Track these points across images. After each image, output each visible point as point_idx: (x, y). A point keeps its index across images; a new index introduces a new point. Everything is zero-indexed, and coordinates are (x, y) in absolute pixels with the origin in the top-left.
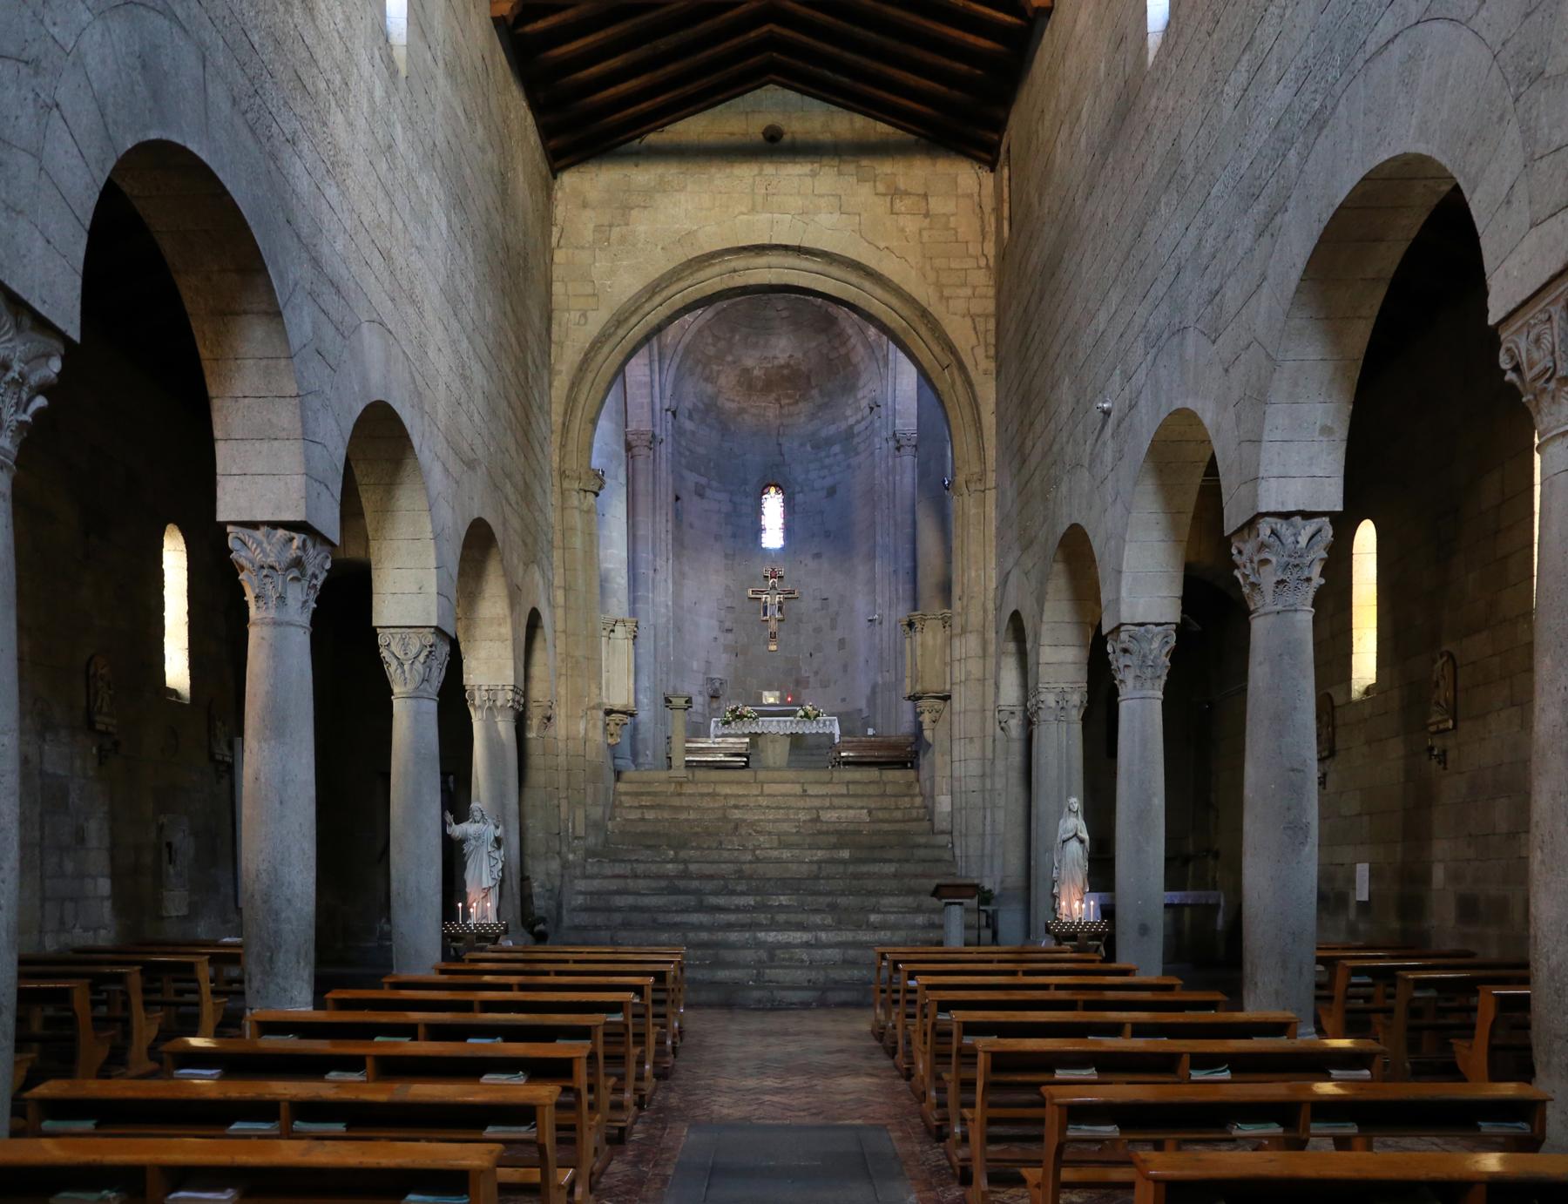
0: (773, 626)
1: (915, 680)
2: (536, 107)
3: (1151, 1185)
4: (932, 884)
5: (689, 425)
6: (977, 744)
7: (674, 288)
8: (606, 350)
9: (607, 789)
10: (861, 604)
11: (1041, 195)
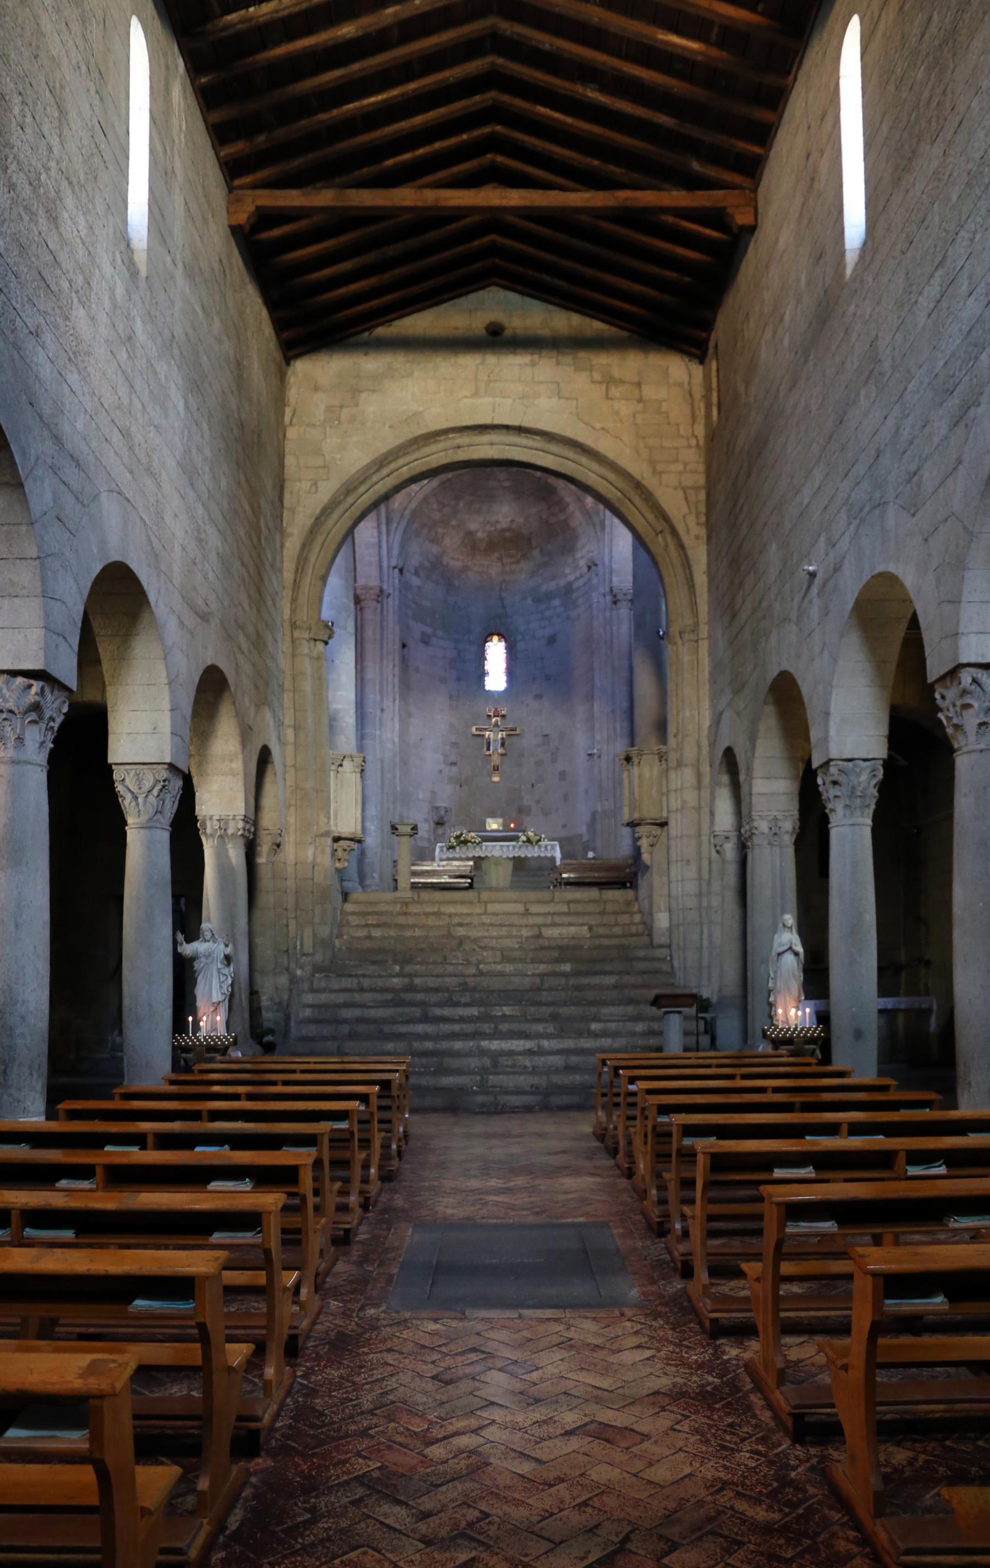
0: (496, 760)
1: (633, 807)
2: (271, 304)
3: (869, 1279)
4: (653, 993)
5: (415, 581)
6: (693, 867)
7: (401, 462)
8: (335, 515)
9: (335, 909)
10: (581, 740)
11: (747, 386)
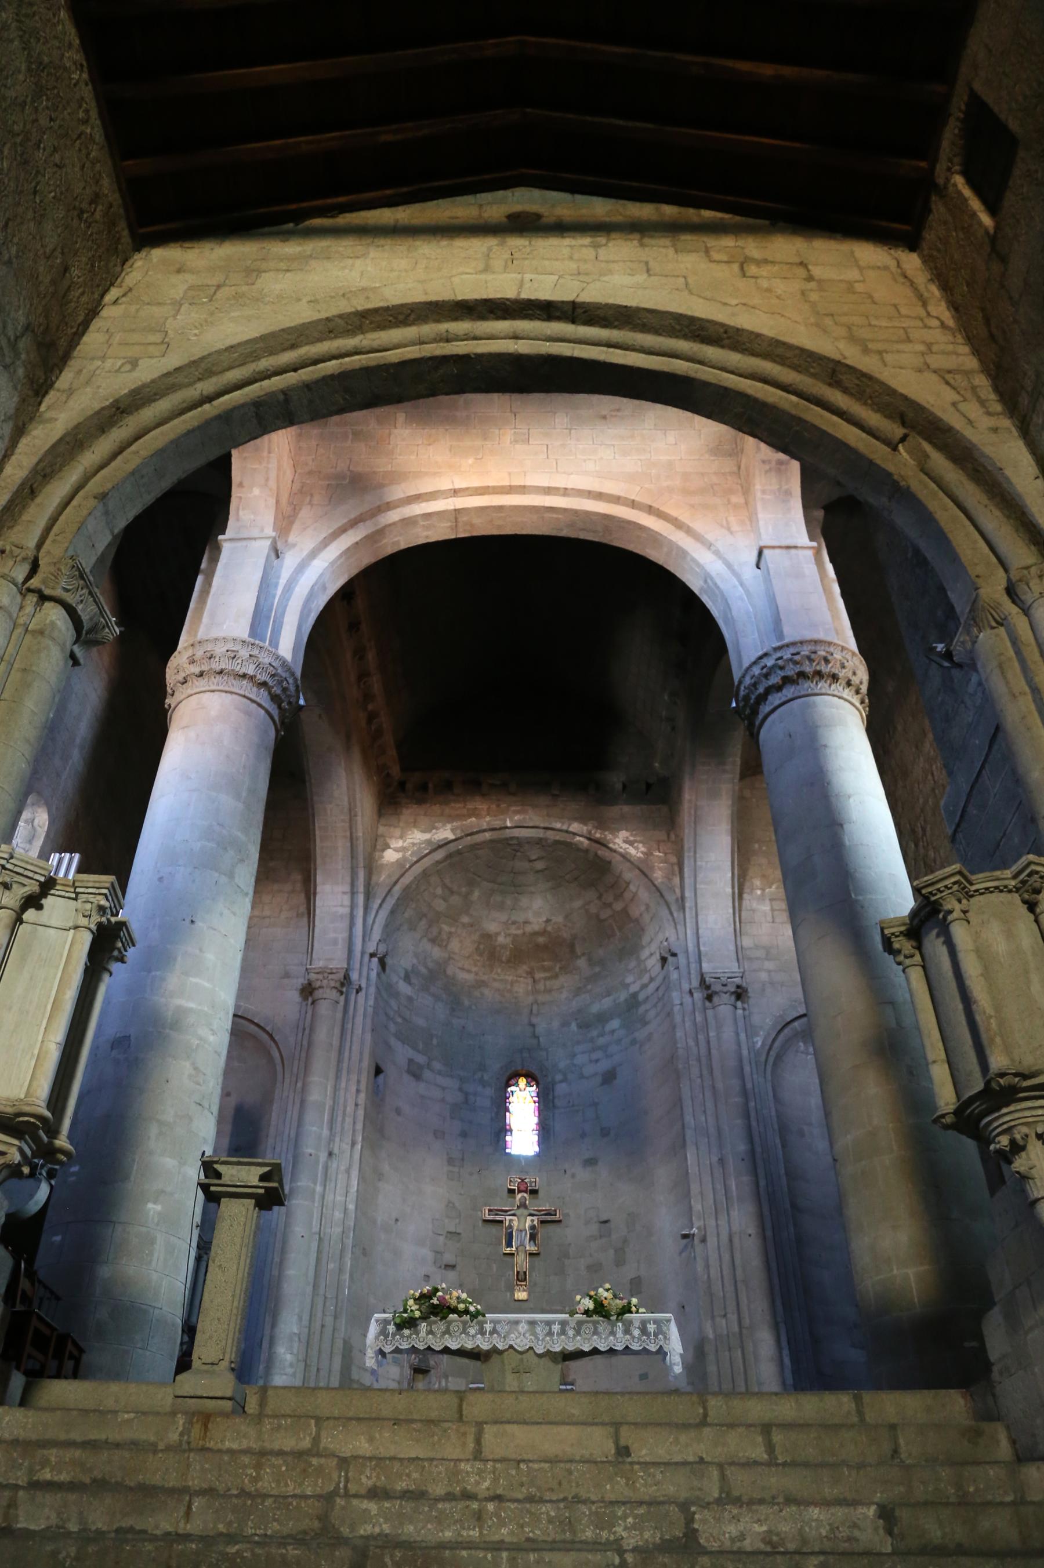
0: (521, 1262)
5: (403, 988)
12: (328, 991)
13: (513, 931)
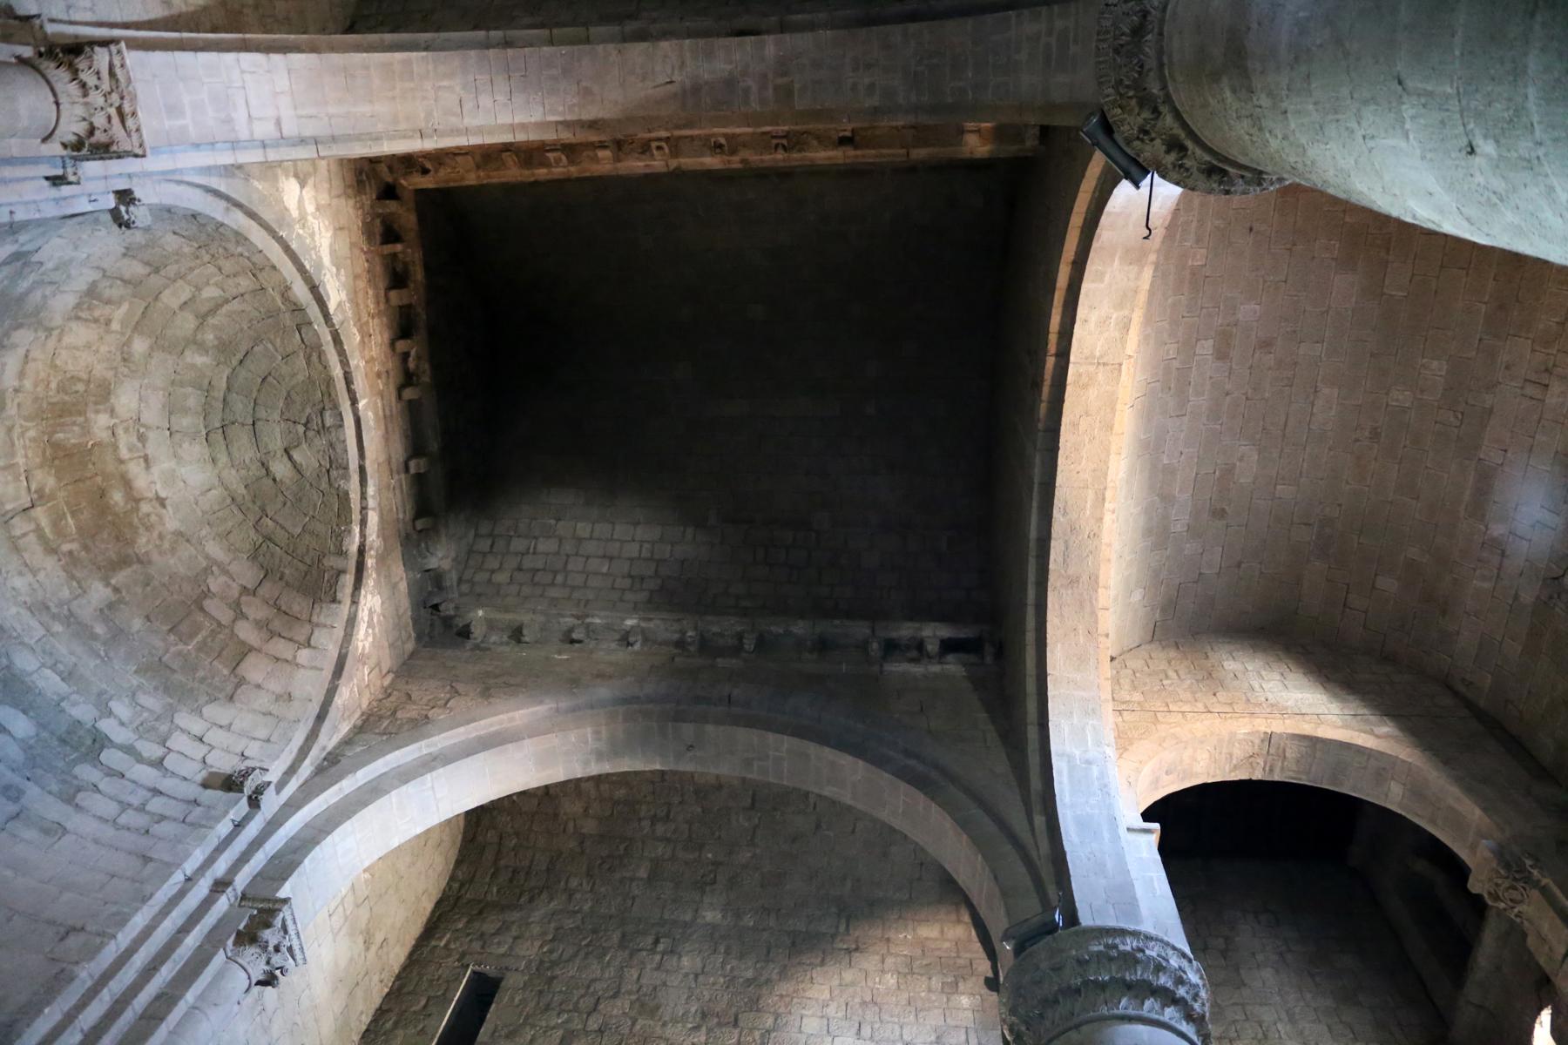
12: (79, 111)
13: (124, 440)
